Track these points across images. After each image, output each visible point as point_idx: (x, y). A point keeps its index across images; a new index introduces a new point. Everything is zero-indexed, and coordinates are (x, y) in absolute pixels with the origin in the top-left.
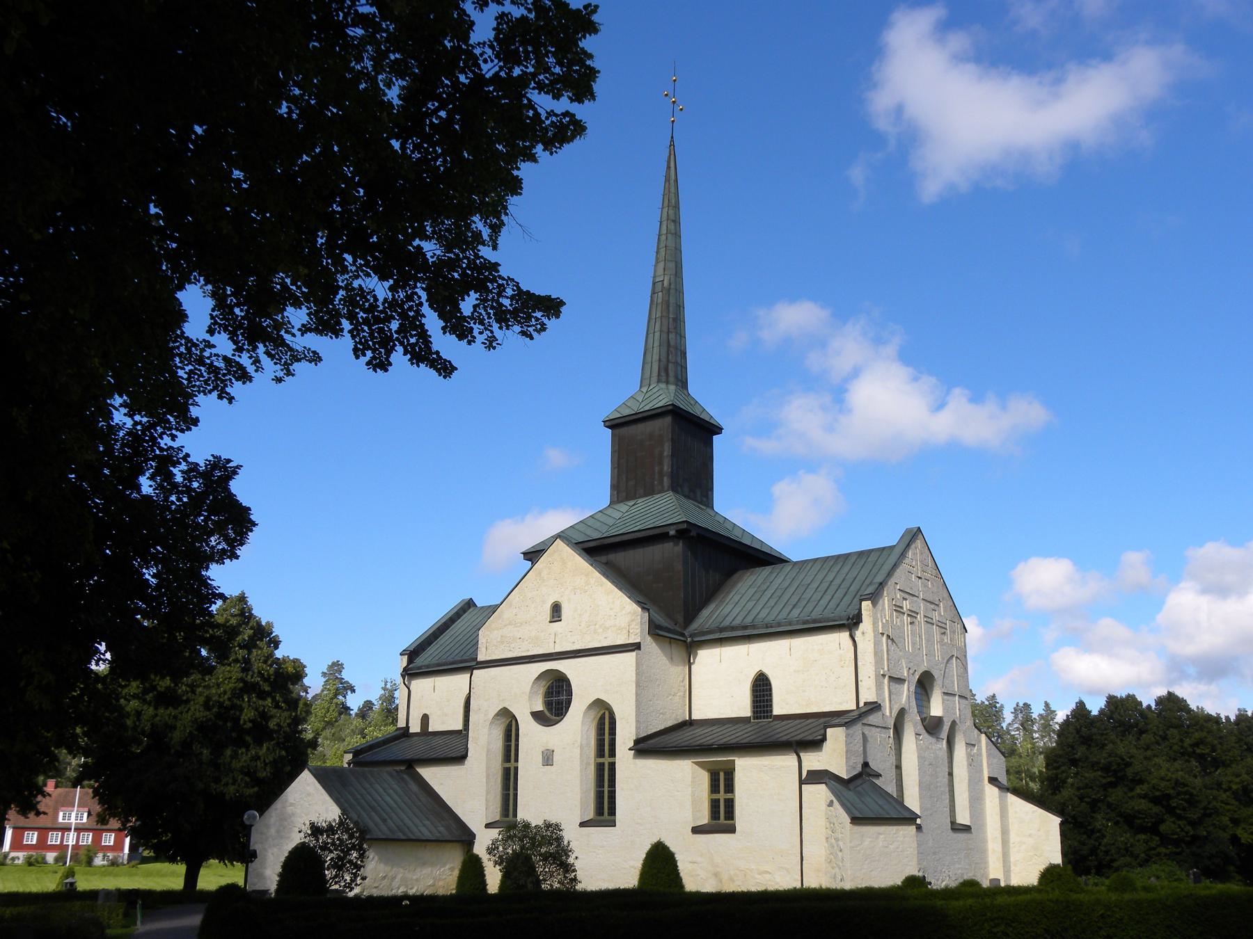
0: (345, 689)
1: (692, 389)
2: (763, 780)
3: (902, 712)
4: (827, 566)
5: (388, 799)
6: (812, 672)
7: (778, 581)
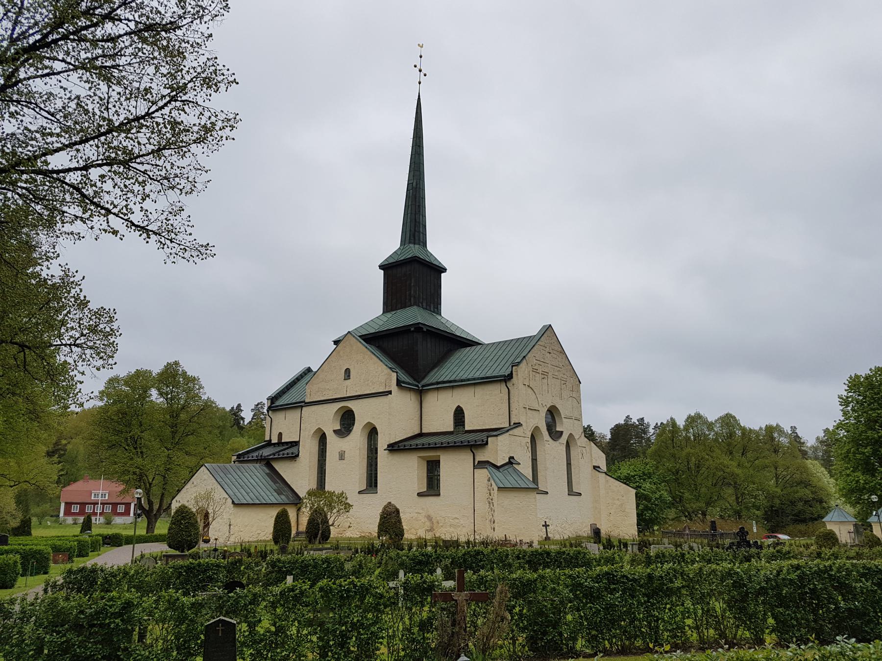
1: (430, 247)
2: (455, 468)
3: (537, 428)
5: (252, 481)
6: (482, 408)
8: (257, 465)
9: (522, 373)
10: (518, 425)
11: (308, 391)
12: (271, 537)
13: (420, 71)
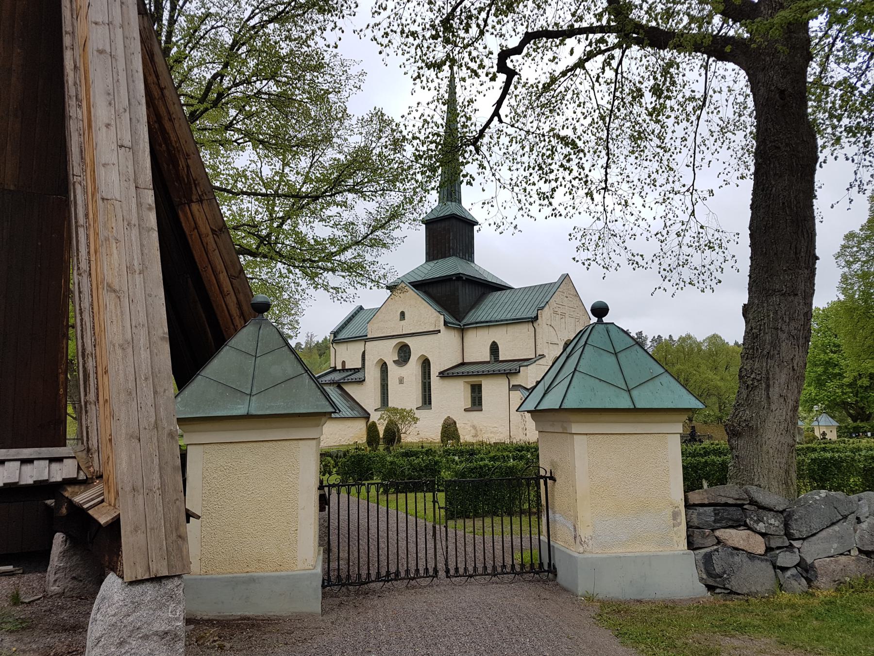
2: (494, 391)
6: (513, 343)
8: (332, 388)
9: (545, 315)
10: (542, 356)
11: (369, 329)
12: (364, 440)
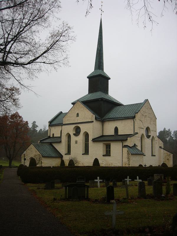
0: (36, 126)
1: (105, 70)
2: (116, 148)
3: (143, 134)
4: (128, 106)
6: (125, 128)
7: (120, 109)
9: (138, 116)
10: (137, 133)
11: (64, 120)
13: (102, 10)
